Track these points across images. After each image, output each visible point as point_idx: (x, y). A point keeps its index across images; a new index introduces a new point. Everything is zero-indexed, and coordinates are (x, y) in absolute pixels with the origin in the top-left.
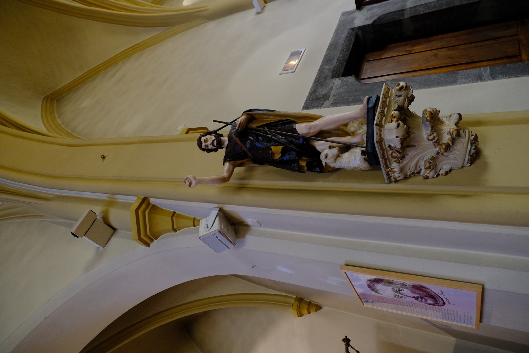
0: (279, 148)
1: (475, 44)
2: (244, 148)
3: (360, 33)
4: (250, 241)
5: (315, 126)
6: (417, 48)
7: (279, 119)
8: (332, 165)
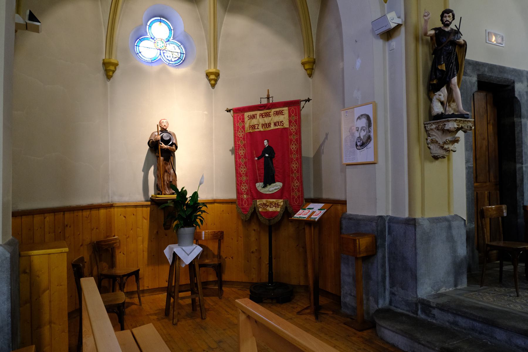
0: (444, 69)
1: (487, 161)
2: (443, 45)
3: (509, 88)
4: (380, 42)
5: (456, 88)
6: (491, 128)
7: (460, 63)
8: (435, 97)
